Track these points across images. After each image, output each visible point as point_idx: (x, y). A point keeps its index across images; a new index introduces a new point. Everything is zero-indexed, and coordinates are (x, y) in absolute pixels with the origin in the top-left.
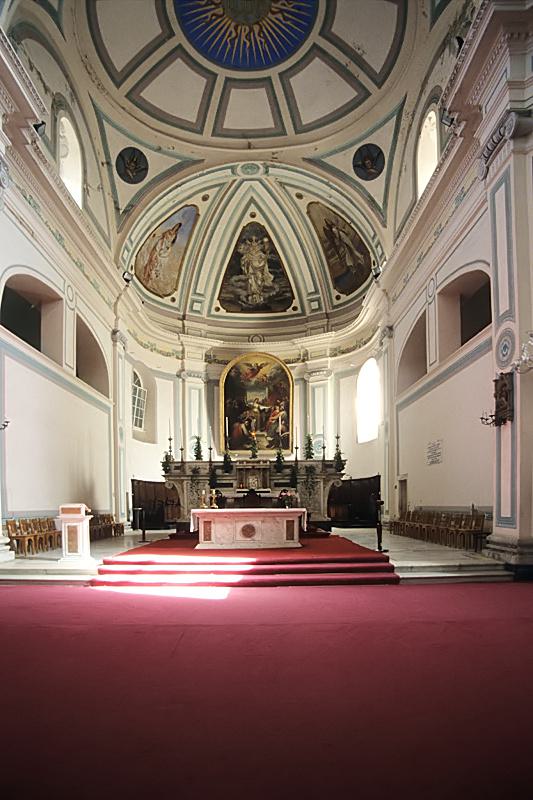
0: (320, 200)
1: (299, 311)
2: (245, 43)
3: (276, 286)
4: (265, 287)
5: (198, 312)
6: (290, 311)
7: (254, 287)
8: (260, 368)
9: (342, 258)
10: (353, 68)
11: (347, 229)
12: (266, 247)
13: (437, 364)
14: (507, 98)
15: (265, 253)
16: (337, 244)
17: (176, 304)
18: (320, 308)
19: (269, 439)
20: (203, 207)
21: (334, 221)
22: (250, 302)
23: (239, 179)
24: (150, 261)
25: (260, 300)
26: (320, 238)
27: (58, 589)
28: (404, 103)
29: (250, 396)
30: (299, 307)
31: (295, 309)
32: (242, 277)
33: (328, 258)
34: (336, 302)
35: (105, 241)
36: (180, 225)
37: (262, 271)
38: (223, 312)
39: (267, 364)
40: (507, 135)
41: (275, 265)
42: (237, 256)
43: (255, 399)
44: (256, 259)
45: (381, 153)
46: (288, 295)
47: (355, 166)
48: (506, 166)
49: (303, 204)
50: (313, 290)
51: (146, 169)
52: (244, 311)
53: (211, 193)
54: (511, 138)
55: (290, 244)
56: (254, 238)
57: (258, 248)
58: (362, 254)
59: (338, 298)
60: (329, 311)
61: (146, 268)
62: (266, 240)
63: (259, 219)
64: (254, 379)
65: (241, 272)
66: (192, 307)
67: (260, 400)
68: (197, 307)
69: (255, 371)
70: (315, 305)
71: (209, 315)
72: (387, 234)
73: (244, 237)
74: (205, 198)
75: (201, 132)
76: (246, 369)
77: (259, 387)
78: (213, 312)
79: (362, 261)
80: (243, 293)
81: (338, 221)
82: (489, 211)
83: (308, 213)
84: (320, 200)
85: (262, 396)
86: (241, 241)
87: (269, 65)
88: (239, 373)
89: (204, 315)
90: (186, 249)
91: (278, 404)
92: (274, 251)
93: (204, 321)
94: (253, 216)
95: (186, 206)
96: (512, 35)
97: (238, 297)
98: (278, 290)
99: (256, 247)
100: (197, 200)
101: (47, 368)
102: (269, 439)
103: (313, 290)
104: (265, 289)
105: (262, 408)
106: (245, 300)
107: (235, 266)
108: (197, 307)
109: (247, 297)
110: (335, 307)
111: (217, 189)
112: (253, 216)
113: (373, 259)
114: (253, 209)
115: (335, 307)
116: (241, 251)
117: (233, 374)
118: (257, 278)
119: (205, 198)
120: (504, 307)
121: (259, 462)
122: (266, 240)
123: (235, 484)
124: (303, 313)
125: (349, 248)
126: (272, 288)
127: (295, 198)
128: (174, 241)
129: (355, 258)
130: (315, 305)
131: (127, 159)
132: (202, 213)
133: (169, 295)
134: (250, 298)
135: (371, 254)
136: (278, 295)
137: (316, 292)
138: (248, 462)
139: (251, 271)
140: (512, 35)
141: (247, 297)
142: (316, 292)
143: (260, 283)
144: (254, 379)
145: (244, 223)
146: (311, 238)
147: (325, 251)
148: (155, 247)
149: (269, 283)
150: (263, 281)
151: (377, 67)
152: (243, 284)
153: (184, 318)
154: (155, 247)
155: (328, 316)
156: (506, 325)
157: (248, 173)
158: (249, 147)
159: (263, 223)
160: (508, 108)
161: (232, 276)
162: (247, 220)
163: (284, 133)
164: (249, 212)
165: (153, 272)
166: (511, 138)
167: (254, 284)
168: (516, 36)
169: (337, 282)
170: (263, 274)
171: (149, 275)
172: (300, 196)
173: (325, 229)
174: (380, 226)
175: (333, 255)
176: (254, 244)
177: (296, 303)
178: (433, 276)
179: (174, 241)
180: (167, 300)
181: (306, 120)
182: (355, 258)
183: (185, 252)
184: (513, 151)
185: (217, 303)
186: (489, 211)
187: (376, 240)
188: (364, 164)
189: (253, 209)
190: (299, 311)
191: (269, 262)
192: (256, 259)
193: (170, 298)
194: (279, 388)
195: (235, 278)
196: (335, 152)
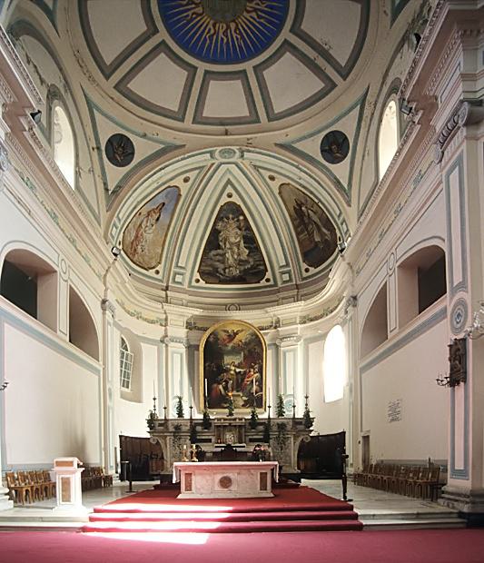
0: (291, 182)
1: (272, 282)
2: (222, 39)
3: (251, 260)
4: (241, 261)
5: (180, 283)
6: (263, 282)
7: (231, 261)
8: (236, 334)
9: (311, 235)
10: (321, 62)
11: (315, 208)
12: (242, 225)
13: (396, 331)
14: (460, 89)
15: (240, 229)
16: (306, 221)
17: (159, 276)
18: (291, 280)
19: (245, 398)
20: (184, 188)
21: (303, 201)
22: (227, 275)
23: (217, 163)
24: (137, 237)
25: (236, 272)
26: (290, 216)
27: (52, 534)
28: (367, 93)
29: (227, 360)
30: (272, 279)
31: (268, 280)
32: (220, 251)
33: (298, 234)
34: (305, 275)
35: (96, 219)
36: (164, 204)
37: (238, 246)
38: (202, 283)
39: (242, 331)
40: (461, 123)
41: (250, 241)
42: (215, 232)
43: (232, 362)
44: (232, 235)
45: (346, 139)
46: (262, 268)
47: (323, 151)
48: (460, 151)
49: (275, 185)
50: (284, 263)
51: (133, 153)
52: (221, 282)
53: (192, 175)
54: (464, 125)
55: (263, 221)
56: (231, 216)
57: (234, 226)
58: (328, 230)
59: (307, 270)
60: (299, 283)
61: (132, 243)
62: (241, 218)
63: (235, 199)
64: (231, 345)
65: (219, 247)
66: (174, 279)
67: (236, 363)
68: (179, 278)
69: (232, 337)
70: (286, 277)
71: (190, 286)
72: (351, 213)
73: (222, 215)
74: (186, 180)
75: (182, 120)
76: (223, 335)
77: (235, 351)
78: (194, 283)
79: (328, 237)
80: (221, 266)
81: (307, 201)
82: (444, 191)
83: (280, 193)
84: (291, 182)
85: (238, 359)
86: (219, 218)
87: (244, 59)
88: (217, 339)
89: (186, 286)
90: (169, 226)
91: (252, 367)
92: (249, 228)
93: (185, 292)
94: (230, 196)
95: (169, 187)
96: (465, 31)
97: (216, 270)
98: (252, 263)
99: (233, 224)
100: (178, 182)
101: (42, 334)
102: (245, 398)
103: (284, 263)
104: (241, 262)
105: (238, 370)
106: (222, 272)
107: (214, 242)
108: (179, 278)
109: (224, 270)
110: (304, 279)
111: (197, 171)
112: (230, 196)
113: (339, 235)
114: (229, 189)
115: (304, 279)
116: (219, 228)
117: (211, 339)
118: (233, 252)
119: (186, 180)
120: (458, 278)
121: (235, 419)
122: (241, 218)
123: (213, 439)
124: (276, 284)
125: (317, 225)
126: (247, 262)
127: (268, 180)
128: (158, 219)
129: (322, 234)
130: (286, 277)
131: (115, 144)
132: (183, 193)
133: (154, 268)
134: (227, 270)
135: (337, 231)
136: (252, 268)
137: (287, 265)
138: (225, 420)
139: (228, 246)
140: (465, 31)
141: (224, 270)
142: (287, 265)
143: (236, 257)
144: (231, 345)
145: (222, 203)
146: (283, 216)
147: (295, 228)
148: (140, 225)
149: (244, 257)
150: (239, 255)
151: (343, 61)
152: (221, 258)
153: (167, 289)
154: (140, 225)
155: (297, 287)
156: (459, 295)
157: (225, 157)
158: (226, 133)
159: (239, 202)
160: (462, 98)
161: (210, 250)
162: (224, 200)
163: (258, 121)
164: (226, 193)
165: (139, 247)
166: (464, 125)
167: (230, 258)
168: (468, 32)
169: (306, 256)
170: (239, 249)
171: (135, 250)
172: (272, 178)
173: (295, 208)
174: (345, 205)
175: (302, 232)
176: (231, 222)
177: (269, 275)
178: (393, 251)
179: (158, 219)
180: (151, 273)
181: (278, 109)
182: (322, 234)
183: (168, 229)
184: (466, 138)
185: (197, 276)
186: (444, 191)
187: (341, 218)
188: (331, 149)
189: (229, 189)
190: (272, 282)
191: (245, 238)
192: (232, 235)
193: (154, 270)
194: (253, 352)
195: (213, 252)
196: (305, 138)
